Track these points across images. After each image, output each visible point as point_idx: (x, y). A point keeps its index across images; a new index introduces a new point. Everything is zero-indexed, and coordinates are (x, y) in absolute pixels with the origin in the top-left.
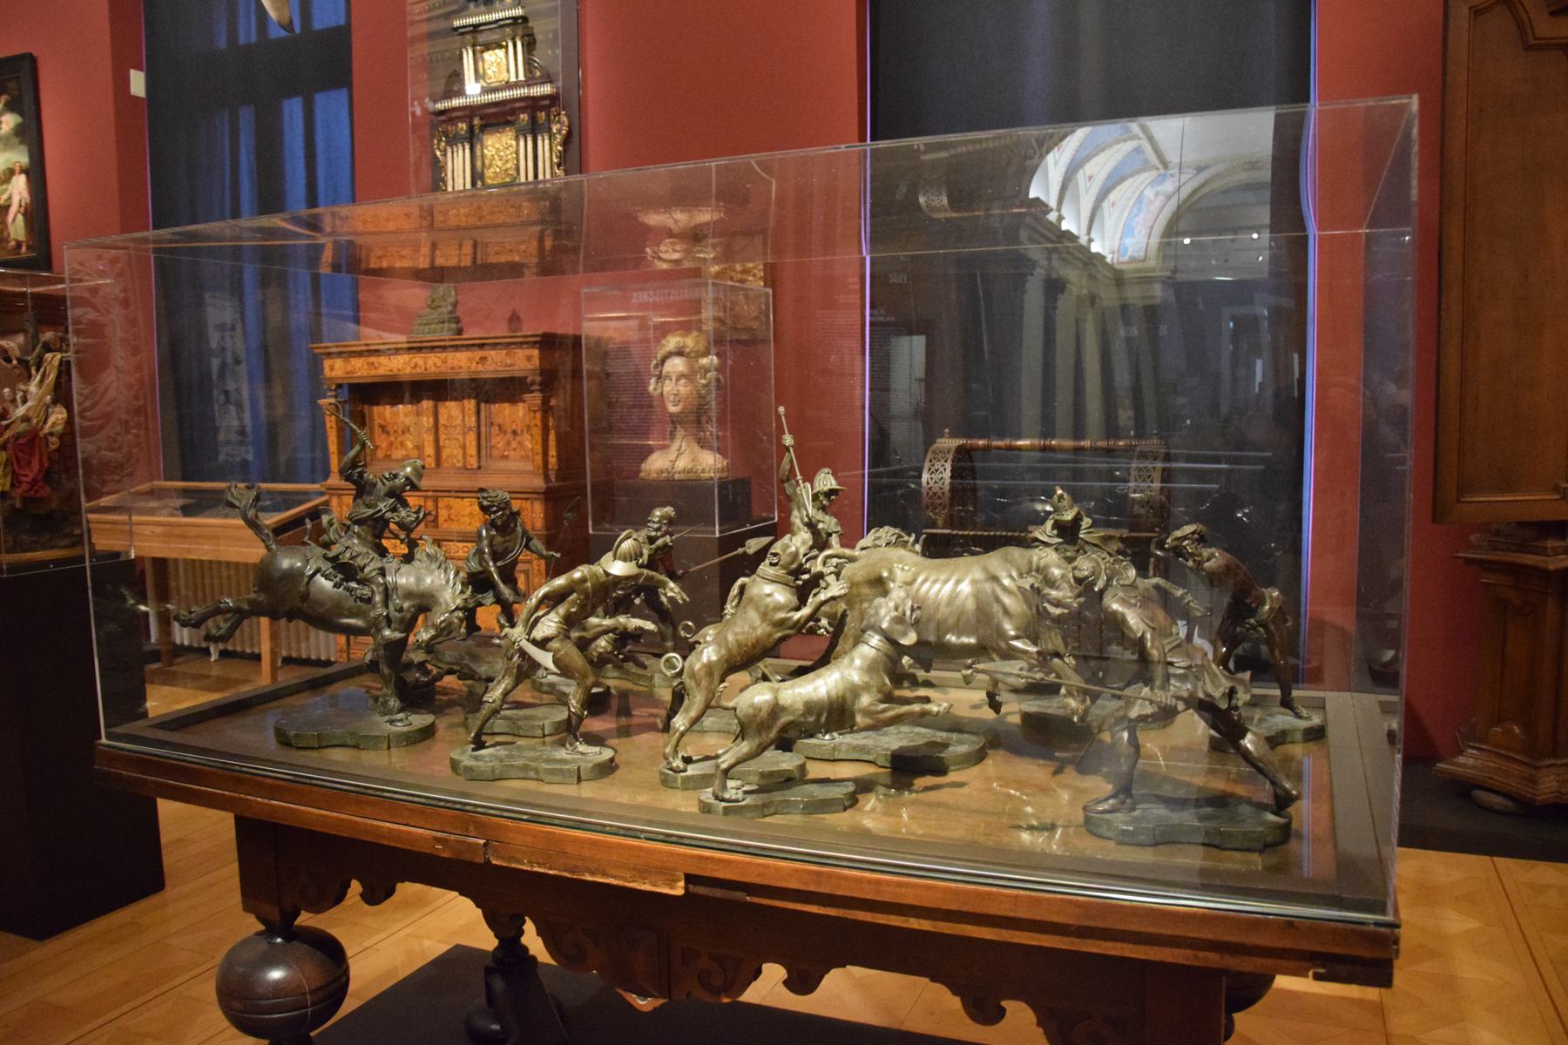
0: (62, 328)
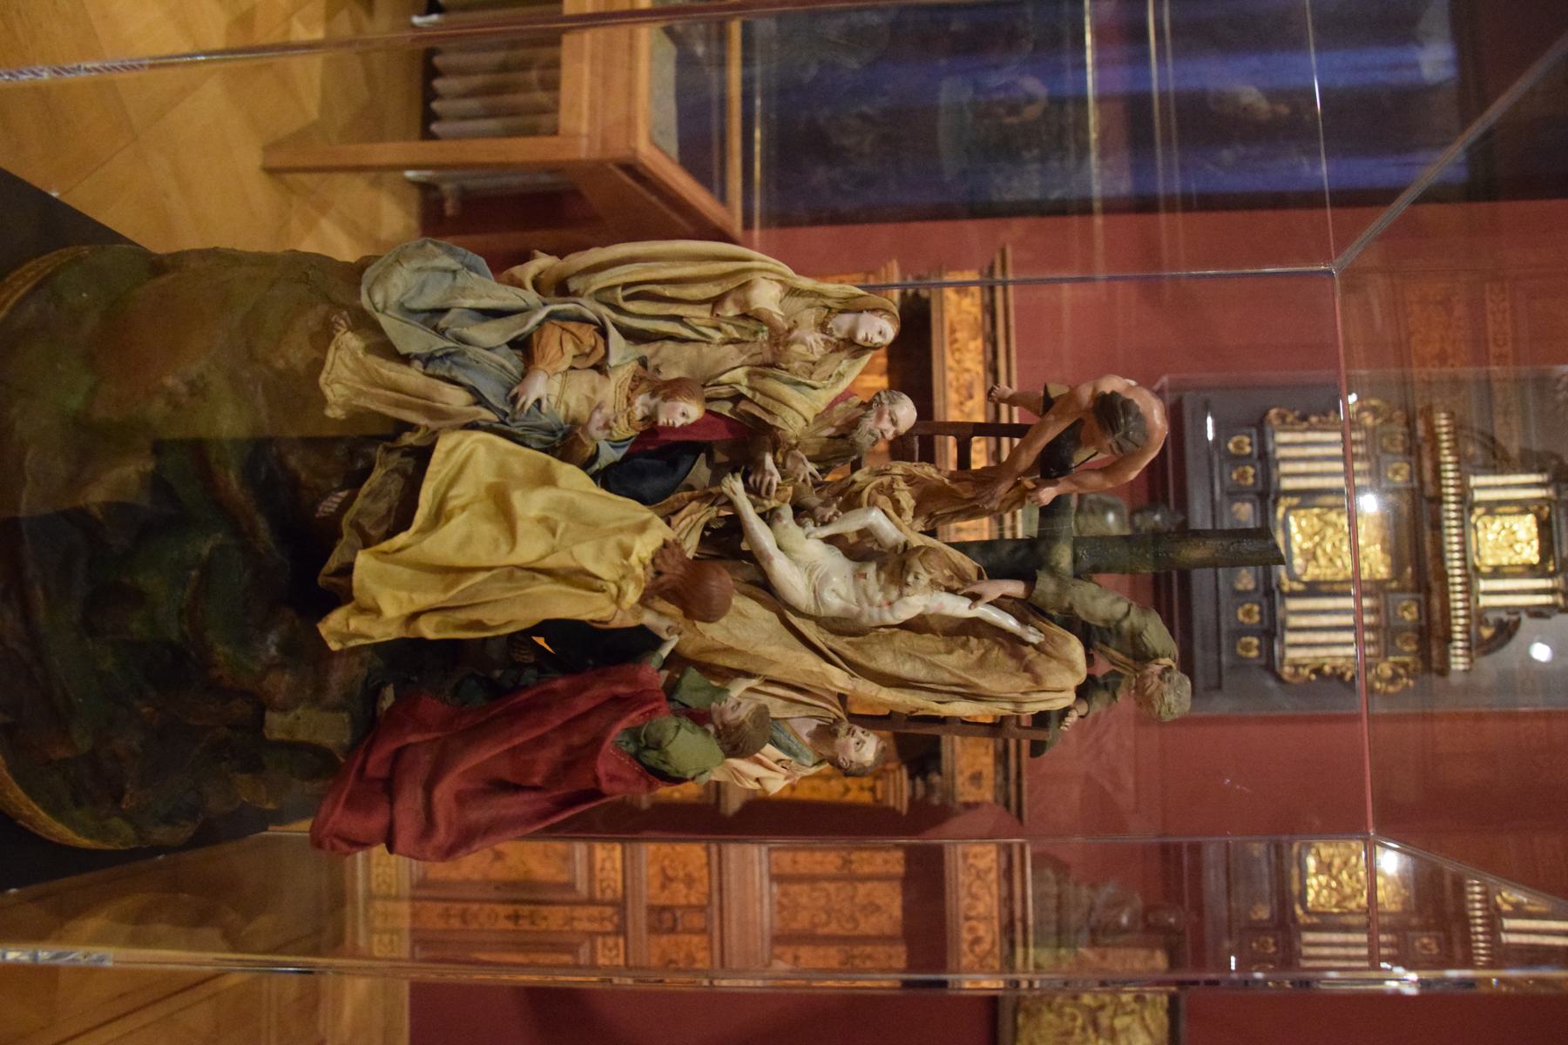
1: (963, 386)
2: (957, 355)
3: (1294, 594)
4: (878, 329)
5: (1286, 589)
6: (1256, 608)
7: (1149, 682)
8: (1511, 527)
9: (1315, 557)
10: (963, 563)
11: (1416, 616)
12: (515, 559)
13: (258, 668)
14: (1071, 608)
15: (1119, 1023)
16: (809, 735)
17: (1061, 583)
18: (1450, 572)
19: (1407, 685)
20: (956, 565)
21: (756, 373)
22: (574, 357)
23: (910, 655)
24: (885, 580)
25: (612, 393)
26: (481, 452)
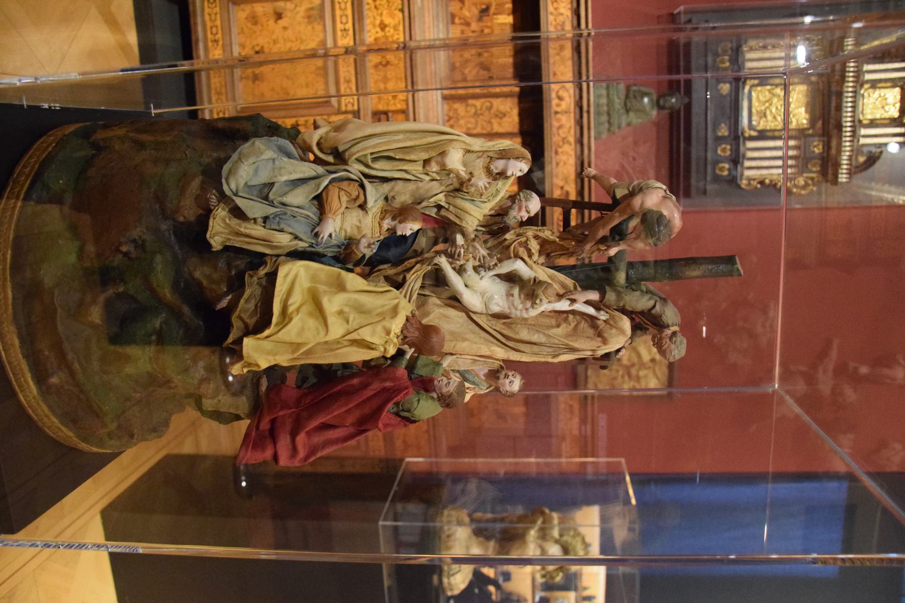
0: (580, 368)
1: (558, 24)
2: (555, 5)
3: (752, 138)
4: (519, 169)
5: (747, 135)
6: (729, 147)
7: (664, 341)
8: (885, 95)
9: (765, 115)
10: (565, 281)
11: (821, 151)
12: (327, 339)
13: (196, 382)
14: (624, 306)
15: (642, 373)
16: (484, 375)
17: (619, 294)
18: (844, 124)
19: (812, 190)
20: (562, 282)
21: (450, 195)
22: (347, 201)
23: (537, 331)
24: (524, 298)
25: (370, 223)
26: (302, 272)
